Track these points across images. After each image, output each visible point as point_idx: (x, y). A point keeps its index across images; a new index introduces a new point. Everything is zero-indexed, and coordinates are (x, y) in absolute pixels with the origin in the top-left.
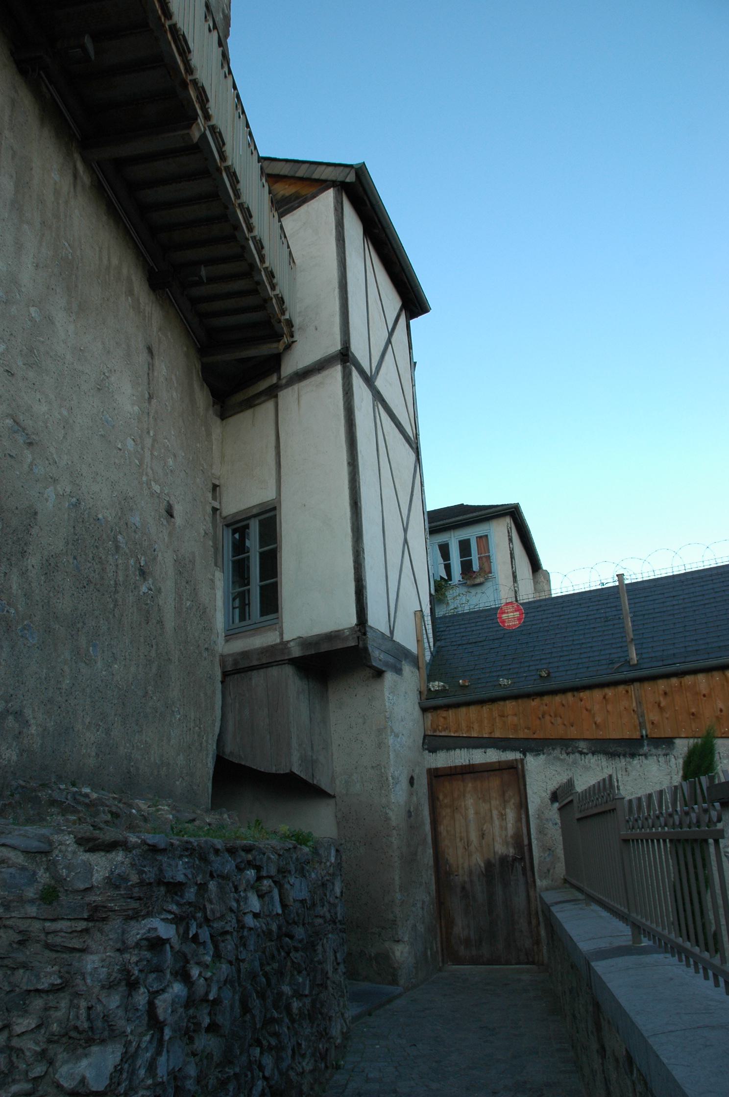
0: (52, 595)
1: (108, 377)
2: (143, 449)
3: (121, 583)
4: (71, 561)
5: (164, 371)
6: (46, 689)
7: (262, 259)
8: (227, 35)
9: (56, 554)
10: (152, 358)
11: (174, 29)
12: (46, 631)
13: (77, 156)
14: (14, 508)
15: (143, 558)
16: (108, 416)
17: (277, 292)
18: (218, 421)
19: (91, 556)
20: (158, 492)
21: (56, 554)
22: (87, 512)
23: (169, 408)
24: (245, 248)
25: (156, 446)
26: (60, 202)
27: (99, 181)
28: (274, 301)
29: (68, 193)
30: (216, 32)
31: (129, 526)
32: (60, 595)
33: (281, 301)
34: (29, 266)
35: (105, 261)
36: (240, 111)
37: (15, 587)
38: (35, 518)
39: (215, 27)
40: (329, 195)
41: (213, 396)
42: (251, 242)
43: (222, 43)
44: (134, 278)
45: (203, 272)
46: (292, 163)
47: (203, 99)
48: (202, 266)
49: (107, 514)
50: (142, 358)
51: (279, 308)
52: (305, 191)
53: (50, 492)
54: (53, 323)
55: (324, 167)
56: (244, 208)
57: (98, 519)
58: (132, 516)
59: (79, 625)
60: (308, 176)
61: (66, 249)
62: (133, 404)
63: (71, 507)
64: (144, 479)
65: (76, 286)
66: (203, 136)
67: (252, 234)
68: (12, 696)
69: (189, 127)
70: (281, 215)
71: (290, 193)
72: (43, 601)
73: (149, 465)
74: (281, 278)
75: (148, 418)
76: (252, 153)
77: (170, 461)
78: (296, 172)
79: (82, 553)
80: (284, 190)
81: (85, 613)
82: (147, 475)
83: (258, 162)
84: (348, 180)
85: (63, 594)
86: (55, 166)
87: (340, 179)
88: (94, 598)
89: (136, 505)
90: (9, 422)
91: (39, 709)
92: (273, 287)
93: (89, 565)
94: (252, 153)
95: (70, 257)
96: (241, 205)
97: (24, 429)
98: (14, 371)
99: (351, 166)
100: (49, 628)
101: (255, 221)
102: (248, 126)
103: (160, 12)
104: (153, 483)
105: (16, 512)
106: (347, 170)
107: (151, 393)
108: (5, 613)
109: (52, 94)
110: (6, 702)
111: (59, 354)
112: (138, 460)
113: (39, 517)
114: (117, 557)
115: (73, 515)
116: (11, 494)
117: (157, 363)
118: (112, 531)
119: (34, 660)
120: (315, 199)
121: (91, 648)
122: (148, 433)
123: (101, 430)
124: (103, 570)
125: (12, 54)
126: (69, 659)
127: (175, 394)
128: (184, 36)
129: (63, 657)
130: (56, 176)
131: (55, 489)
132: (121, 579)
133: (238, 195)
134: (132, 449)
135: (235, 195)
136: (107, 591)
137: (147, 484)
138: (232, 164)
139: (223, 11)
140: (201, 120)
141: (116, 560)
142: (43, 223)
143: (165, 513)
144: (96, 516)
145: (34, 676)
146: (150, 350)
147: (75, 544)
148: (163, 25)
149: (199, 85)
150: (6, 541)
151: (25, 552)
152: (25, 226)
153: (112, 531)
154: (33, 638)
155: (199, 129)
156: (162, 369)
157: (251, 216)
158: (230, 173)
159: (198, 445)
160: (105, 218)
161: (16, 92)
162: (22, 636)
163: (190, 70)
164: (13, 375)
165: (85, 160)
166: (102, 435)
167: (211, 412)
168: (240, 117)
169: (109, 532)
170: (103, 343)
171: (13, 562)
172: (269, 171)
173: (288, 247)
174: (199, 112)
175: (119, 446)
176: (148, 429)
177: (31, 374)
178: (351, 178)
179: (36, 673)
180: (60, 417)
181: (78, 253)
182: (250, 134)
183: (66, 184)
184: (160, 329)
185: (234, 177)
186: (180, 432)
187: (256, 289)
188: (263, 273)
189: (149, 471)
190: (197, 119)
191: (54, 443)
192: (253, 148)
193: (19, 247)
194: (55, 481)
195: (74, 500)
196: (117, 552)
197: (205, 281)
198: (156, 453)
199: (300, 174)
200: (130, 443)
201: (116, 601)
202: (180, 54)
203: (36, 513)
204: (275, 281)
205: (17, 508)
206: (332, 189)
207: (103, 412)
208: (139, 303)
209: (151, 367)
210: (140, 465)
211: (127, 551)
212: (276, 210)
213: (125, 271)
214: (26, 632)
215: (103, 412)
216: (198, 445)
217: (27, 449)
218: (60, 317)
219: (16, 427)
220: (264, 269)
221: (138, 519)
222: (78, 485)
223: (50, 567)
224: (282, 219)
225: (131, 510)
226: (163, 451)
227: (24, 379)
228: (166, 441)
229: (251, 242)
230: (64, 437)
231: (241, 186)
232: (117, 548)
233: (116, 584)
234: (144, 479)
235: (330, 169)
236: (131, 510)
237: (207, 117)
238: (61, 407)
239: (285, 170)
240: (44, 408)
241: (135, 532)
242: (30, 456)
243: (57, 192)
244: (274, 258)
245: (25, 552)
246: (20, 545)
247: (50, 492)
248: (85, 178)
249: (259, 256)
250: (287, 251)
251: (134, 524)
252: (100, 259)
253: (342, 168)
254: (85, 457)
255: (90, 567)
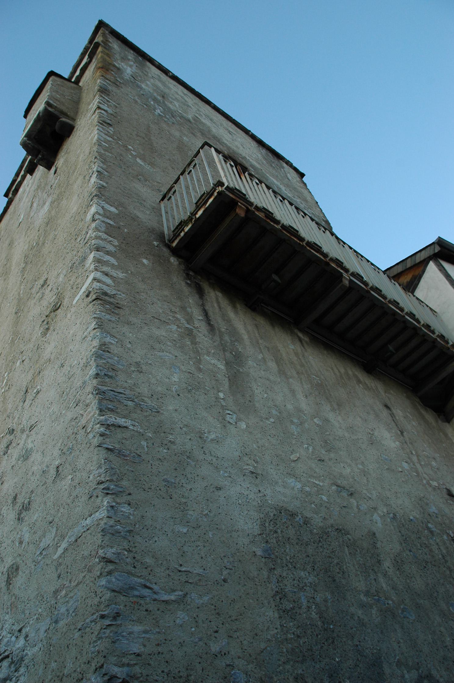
0: (408, 581)
1: (373, 434)
2: (414, 465)
3: (446, 554)
4: (409, 553)
5: (401, 413)
6: (437, 650)
7: (418, 321)
8: (331, 228)
9: (398, 554)
10: (390, 410)
11: (309, 244)
12: (416, 607)
13: (296, 331)
14: (361, 536)
15: (451, 532)
16: (385, 456)
17: (437, 333)
18: (447, 424)
19: (419, 545)
20: (437, 485)
21: (398, 554)
22: (402, 519)
23: (415, 433)
24: (405, 322)
25: (420, 458)
26: (300, 357)
27: (313, 336)
28: (438, 339)
29: (302, 351)
30: (307, 216)
31: (432, 516)
32: (413, 579)
33: (442, 337)
34: (302, 399)
35: (338, 374)
36: (360, 257)
37: (384, 585)
38: (375, 537)
39: (325, 229)
40: (432, 266)
41: (435, 412)
42: (407, 317)
43: (332, 234)
44: (356, 373)
45: (391, 348)
46: (401, 263)
47: (339, 263)
48: (389, 345)
49: (415, 514)
50: (385, 413)
51: (443, 341)
52: (417, 272)
53: (376, 517)
54: (329, 421)
55: (419, 254)
56: (392, 302)
57: (411, 520)
58: (429, 508)
59: (435, 594)
60: (414, 264)
61: (316, 379)
62: (394, 442)
63: (392, 520)
64: (425, 482)
65: (331, 395)
66: (351, 281)
67: (405, 312)
68: (418, 664)
69: (341, 281)
70: (413, 292)
71: (410, 279)
72: (405, 588)
73: (423, 472)
74: (434, 324)
75: (407, 445)
76: (379, 272)
77: (434, 463)
78: (406, 266)
79: (413, 546)
80: (406, 279)
81: (434, 585)
82: (425, 479)
83: (385, 274)
84: (436, 251)
85: (415, 577)
86: (289, 342)
87: (432, 253)
88: (435, 572)
89: (428, 500)
90: (334, 488)
91: (440, 668)
92: (433, 332)
93: (420, 551)
94: (379, 272)
95: (320, 382)
96: (390, 302)
97: (344, 488)
98: (323, 458)
99: (433, 243)
100: (417, 604)
101: (402, 304)
102: (368, 261)
103: (298, 241)
104: (431, 482)
105: (363, 538)
106: (433, 247)
107: (400, 429)
108: (387, 605)
109: (270, 310)
110: (417, 670)
111: (341, 436)
112: (415, 472)
113: (377, 535)
114: (434, 538)
115: (395, 524)
116: (355, 529)
117: (394, 411)
118: (423, 524)
119: (419, 631)
120: (425, 273)
121: (451, 608)
122: (412, 453)
123: (385, 466)
124: (430, 551)
125: (246, 305)
126: (441, 621)
127: (414, 423)
128: (314, 243)
129: (436, 622)
130: (292, 347)
131: (378, 514)
132: (444, 551)
133: (385, 297)
134: (408, 468)
135: (383, 298)
136: (440, 564)
137: (428, 484)
138: (373, 284)
139: (324, 220)
140: (345, 275)
141: (435, 540)
142: (298, 373)
143: (448, 497)
144: (409, 519)
145: (425, 643)
146: (387, 406)
147: (406, 542)
148: (303, 246)
149: (334, 259)
150: (366, 559)
151: (380, 560)
152: (291, 380)
153: (423, 524)
154: (411, 615)
155: (347, 279)
156: (399, 413)
157: (398, 304)
158: (374, 289)
159: (444, 445)
160: (325, 352)
161: (256, 320)
162: (404, 617)
163: (325, 255)
164: (323, 461)
165: (301, 331)
166: (387, 469)
167: (440, 422)
168: (362, 260)
169: (422, 525)
170: (360, 417)
171: (376, 570)
172: (392, 275)
173: (428, 306)
174: (342, 271)
175: (400, 470)
176: (410, 451)
177: (332, 455)
178: (437, 249)
179: (425, 640)
180: (359, 471)
181: (322, 377)
182: (372, 264)
183: (298, 347)
184: (385, 392)
185: (378, 290)
186: (429, 443)
187: (425, 339)
188: (423, 328)
189: (425, 476)
190: (343, 275)
191: (364, 488)
192: (377, 270)
193: (293, 392)
194: (375, 509)
195: (391, 515)
196: (433, 535)
197: (395, 352)
198: (423, 463)
199: (409, 265)
200: (405, 465)
201: (449, 568)
202: (317, 252)
203: (374, 534)
204: (432, 329)
205: (362, 536)
206: (431, 261)
207: (380, 455)
208: (367, 385)
209: (393, 416)
210: (418, 475)
211: (439, 532)
212: (409, 292)
213: (350, 373)
214: (405, 613)
215: (380, 455)
216: (444, 445)
217: (351, 498)
218: (331, 416)
219: (339, 489)
220: (422, 326)
221: (434, 508)
222: (389, 505)
223: (398, 564)
224: (415, 294)
225: (427, 504)
226: (426, 459)
227: (330, 459)
228: (425, 452)
229: (407, 317)
230: (367, 481)
231: (384, 292)
232: (432, 532)
233: (443, 556)
234: (425, 482)
235: (423, 252)
236: (427, 504)
237: (347, 271)
238: (357, 464)
239: (400, 269)
240: (348, 470)
241: (437, 517)
242: (354, 501)
243: (296, 354)
244: (424, 317)
245: (380, 560)
246: (375, 558)
247: (376, 517)
248: (306, 339)
249: (415, 321)
250: (428, 308)
251: (434, 512)
252: (335, 374)
253: (429, 248)
254: (384, 486)
255: (422, 553)
